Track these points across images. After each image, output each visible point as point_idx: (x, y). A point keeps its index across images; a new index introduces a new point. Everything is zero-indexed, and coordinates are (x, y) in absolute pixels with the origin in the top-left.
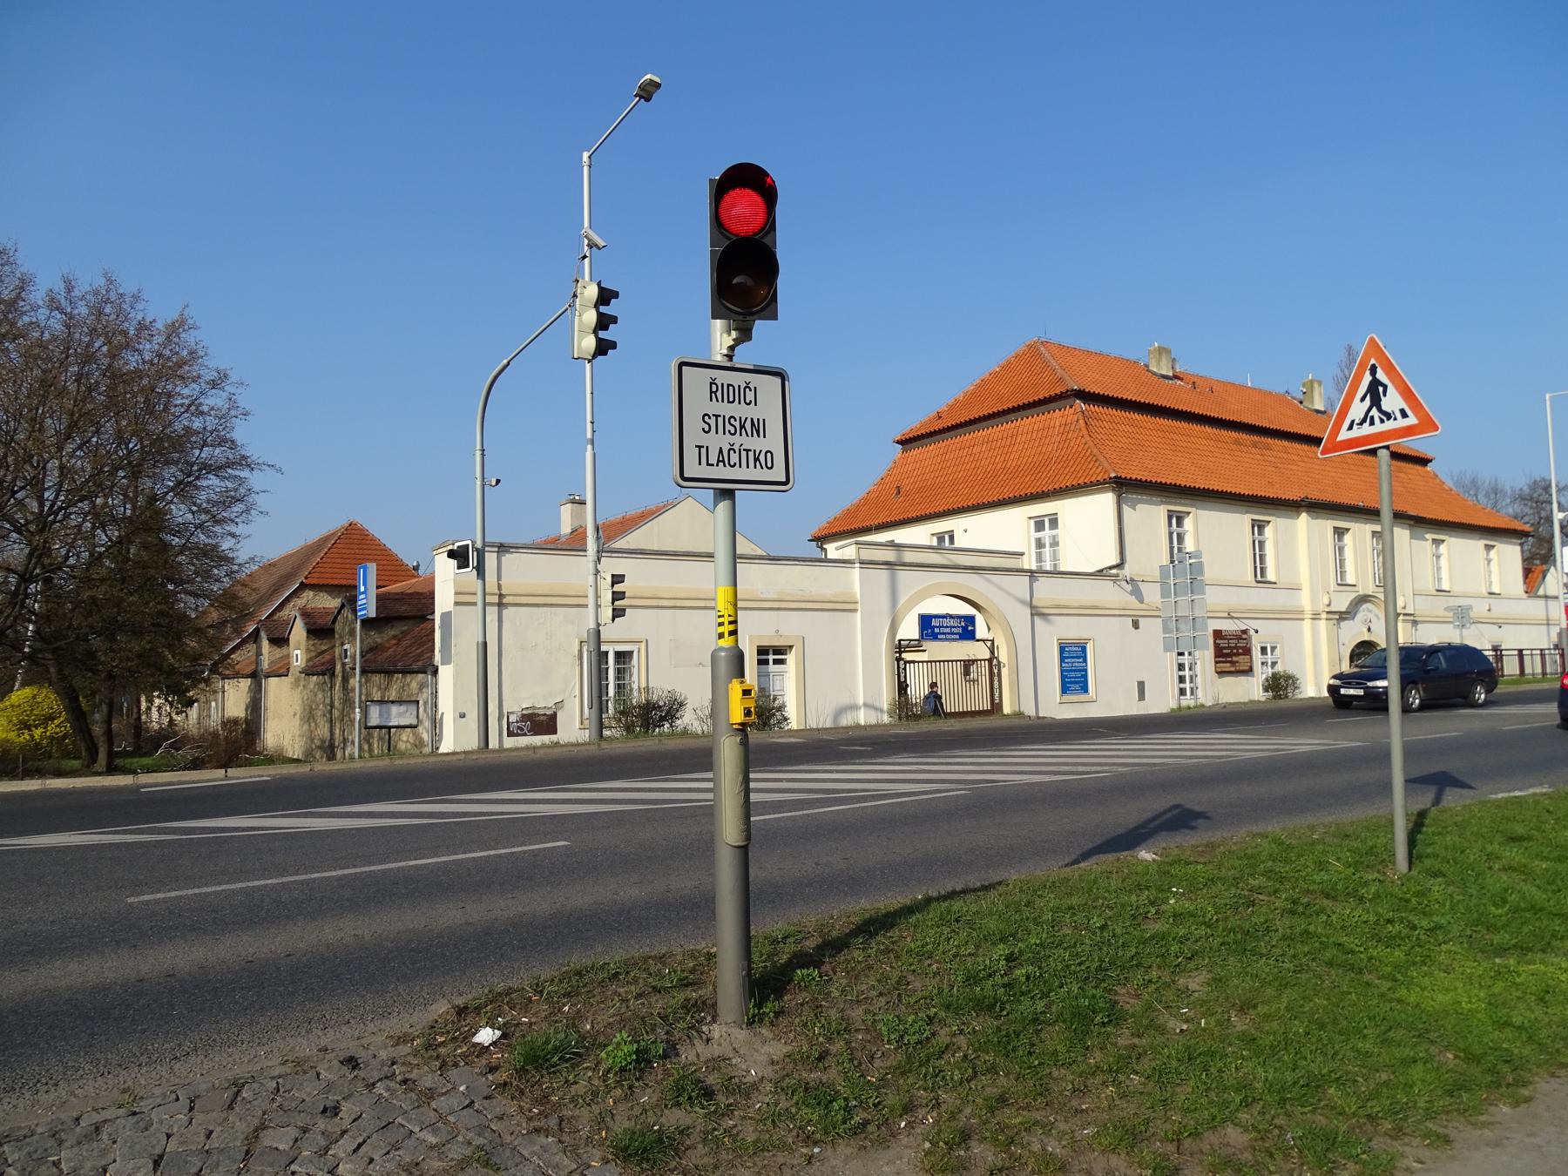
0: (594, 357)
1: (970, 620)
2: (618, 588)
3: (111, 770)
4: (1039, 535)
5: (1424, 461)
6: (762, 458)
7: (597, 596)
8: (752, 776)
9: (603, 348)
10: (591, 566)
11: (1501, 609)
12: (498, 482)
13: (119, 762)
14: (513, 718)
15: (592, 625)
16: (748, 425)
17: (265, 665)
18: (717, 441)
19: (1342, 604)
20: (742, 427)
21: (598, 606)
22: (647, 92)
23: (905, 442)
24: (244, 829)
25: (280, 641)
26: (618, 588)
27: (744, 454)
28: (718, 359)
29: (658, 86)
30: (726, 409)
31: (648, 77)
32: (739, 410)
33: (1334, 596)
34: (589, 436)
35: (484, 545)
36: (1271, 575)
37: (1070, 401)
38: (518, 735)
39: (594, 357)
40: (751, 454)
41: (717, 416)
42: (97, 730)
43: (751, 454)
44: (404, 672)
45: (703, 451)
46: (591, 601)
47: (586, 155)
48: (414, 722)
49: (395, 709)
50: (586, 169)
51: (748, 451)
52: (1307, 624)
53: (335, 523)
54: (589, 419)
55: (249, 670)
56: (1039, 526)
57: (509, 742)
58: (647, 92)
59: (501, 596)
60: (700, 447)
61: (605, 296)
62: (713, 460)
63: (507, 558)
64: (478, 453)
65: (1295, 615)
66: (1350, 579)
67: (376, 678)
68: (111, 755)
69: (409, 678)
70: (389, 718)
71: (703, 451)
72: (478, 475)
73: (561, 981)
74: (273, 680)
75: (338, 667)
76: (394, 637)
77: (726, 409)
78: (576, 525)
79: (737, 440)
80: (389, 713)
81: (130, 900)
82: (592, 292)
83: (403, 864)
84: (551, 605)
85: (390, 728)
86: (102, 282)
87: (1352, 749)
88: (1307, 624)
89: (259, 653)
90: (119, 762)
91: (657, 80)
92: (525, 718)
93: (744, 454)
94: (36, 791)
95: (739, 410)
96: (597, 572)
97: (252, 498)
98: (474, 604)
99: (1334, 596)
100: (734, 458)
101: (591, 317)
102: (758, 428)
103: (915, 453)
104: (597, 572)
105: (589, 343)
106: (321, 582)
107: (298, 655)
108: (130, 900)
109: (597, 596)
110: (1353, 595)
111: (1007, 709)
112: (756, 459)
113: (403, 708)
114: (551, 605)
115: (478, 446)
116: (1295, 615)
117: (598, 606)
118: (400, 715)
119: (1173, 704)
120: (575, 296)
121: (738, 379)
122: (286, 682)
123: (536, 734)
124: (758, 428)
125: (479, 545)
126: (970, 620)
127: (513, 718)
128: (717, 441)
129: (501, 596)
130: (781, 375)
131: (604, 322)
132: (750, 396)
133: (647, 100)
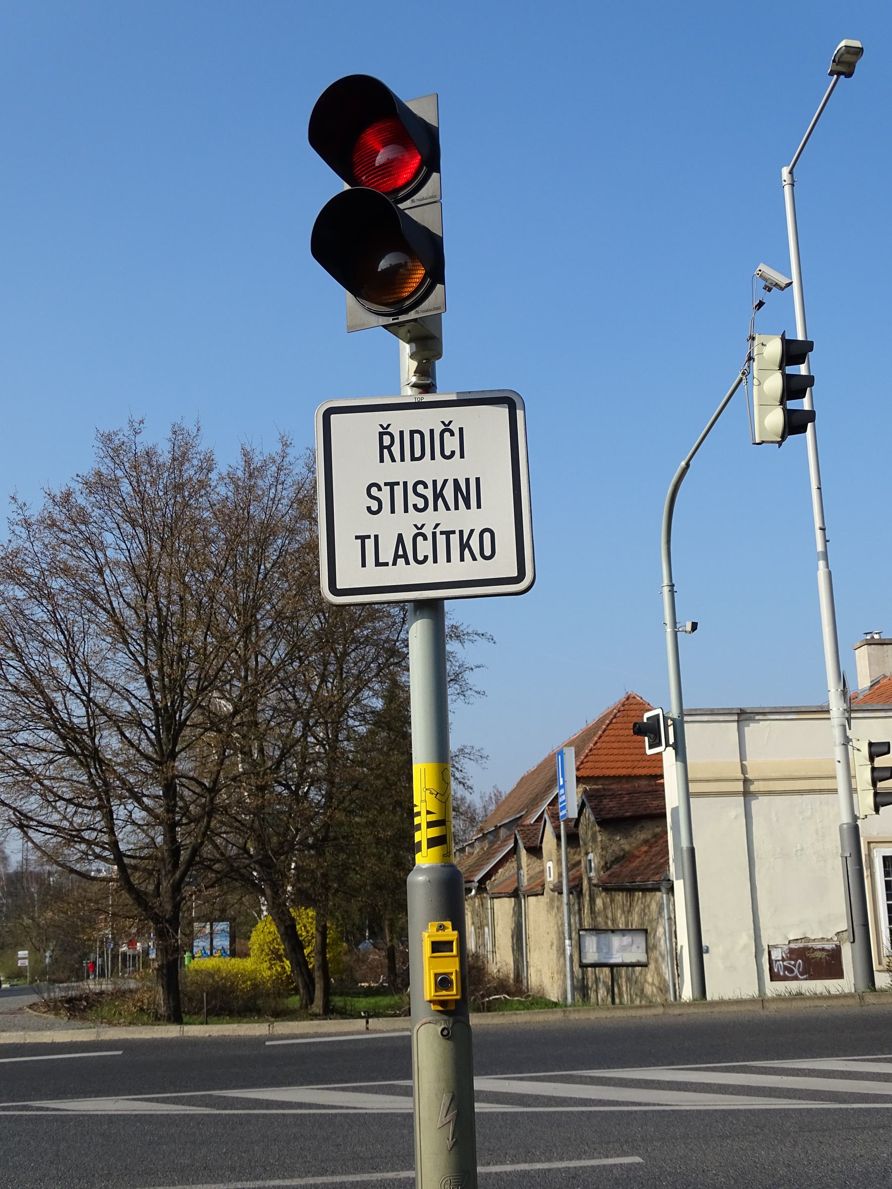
0: (783, 437)
2: (880, 762)
3: (329, 1012)
6: (474, 543)
7: (850, 777)
8: (481, 1084)
9: (795, 423)
10: (837, 733)
12: (694, 626)
13: (338, 1001)
14: (777, 955)
15: (846, 819)
16: (449, 493)
17: (525, 881)
18: (391, 526)
20: (438, 495)
21: (852, 791)
22: (846, 65)
24: (301, 1105)
25: (535, 851)
26: (880, 762)
27: (441, 540)
28: (409, 394)
29: (859, 52)
30: (407, 471)
31: (843, 44)
32: (432, 470)
34: (820, 548)
35: (682, 714)
38: (785, 979)
39: (783, 437)
40: (455, 539)
41: (392, 485)
42: (313, 963)
43: (455, 539)
44: (645, 890)
45: (370, 544)
46: (841, 784)
47: (785, 171)
48: (643, 958)
49: (617, 941)
50: (787, 190)
51: (448, 534)
53: (620, 697)
54: (818, 524)
55: (510, 890)
57: (774, 988)
58: (846, 65)
59: (746, 781)
60: (363, 538)
61: (794, 352)
62: (387, 555)
63: (752, 730)
64: (666, 590)
67: (620, 897)
68: (328, 992)
69: (649, 895)
70: (609, 953)
71: (370, 544)
72: (668, 619)
74: (532, 899)
75: (585, 883)
76: (646, 842)
77: (407, 471)
78: (877, 675)
79: (429, 518)
80: (609, 947)
81: (637, 1159)
82: (773, 348)
83: (391, 1175)
84: (821, 791)
85: (612, 966)
86: (279, 447)
89: (519, 867)
90: (338, 1001)
91: (857, 44)
92: (794, 954)
93: (441, 540)
94: (172, 1039)
95: (432, 470)
96: (847, 741)
97: (467, 675)
98: (835, 791)
100: (425, 548)
101: (774, 383)
102: (466, 494)
104: (847, 741)
105: (775, 419)
106: (596, 772)
107: (551, 869)
108: (637, 1159)
109: (850, 777)
112: (464, 545)
113: (627, 940)
114: (821, 791)
115: (666, 581)
117: (852, 791)
118: (623, 949)
119: (750, 990)
120: (751, 358)
121: (428, 420)
122: (543, 900)
123: (812, 977)
124: (466, 494)
125: (674, 713)
127: (777, 955)
128: (391, 526)
129: (746, 781)
130: (509, 402)
131: (794, 388)
132: (451, 443)
133: (849, 75)
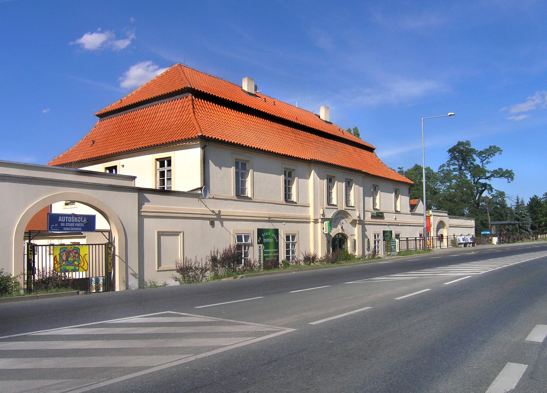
1: (91, 220)
4: (162, 169)
5: (371, 150)
11: (401, 219)
19: (330, 214)
23: (102, 116)
33: (325, 210)
36: (294, 198)
37: (186, 95)
38: (384, 235)
52: (312, 224)
56: (162, 165)
65: (306, 221)
66: (334, 202)
73: (477, 215)
87: (379, 276)
88: (312, 224)
99: (325, 210)
103: (107, 121)
110: (336, 210)
111: (118, 287)
116: (306, 221)
126: (91, 220)
